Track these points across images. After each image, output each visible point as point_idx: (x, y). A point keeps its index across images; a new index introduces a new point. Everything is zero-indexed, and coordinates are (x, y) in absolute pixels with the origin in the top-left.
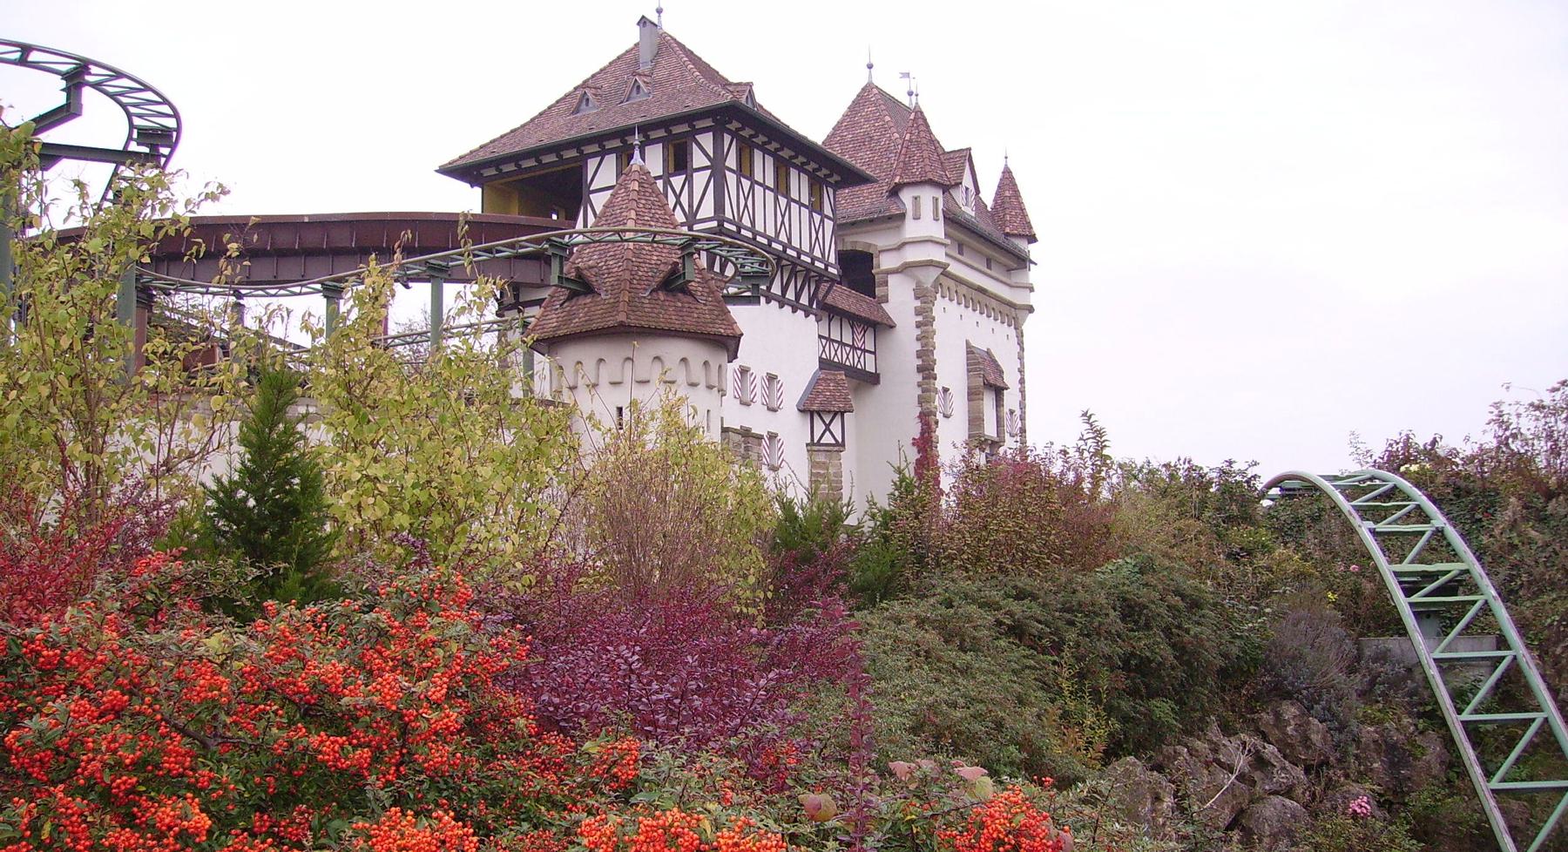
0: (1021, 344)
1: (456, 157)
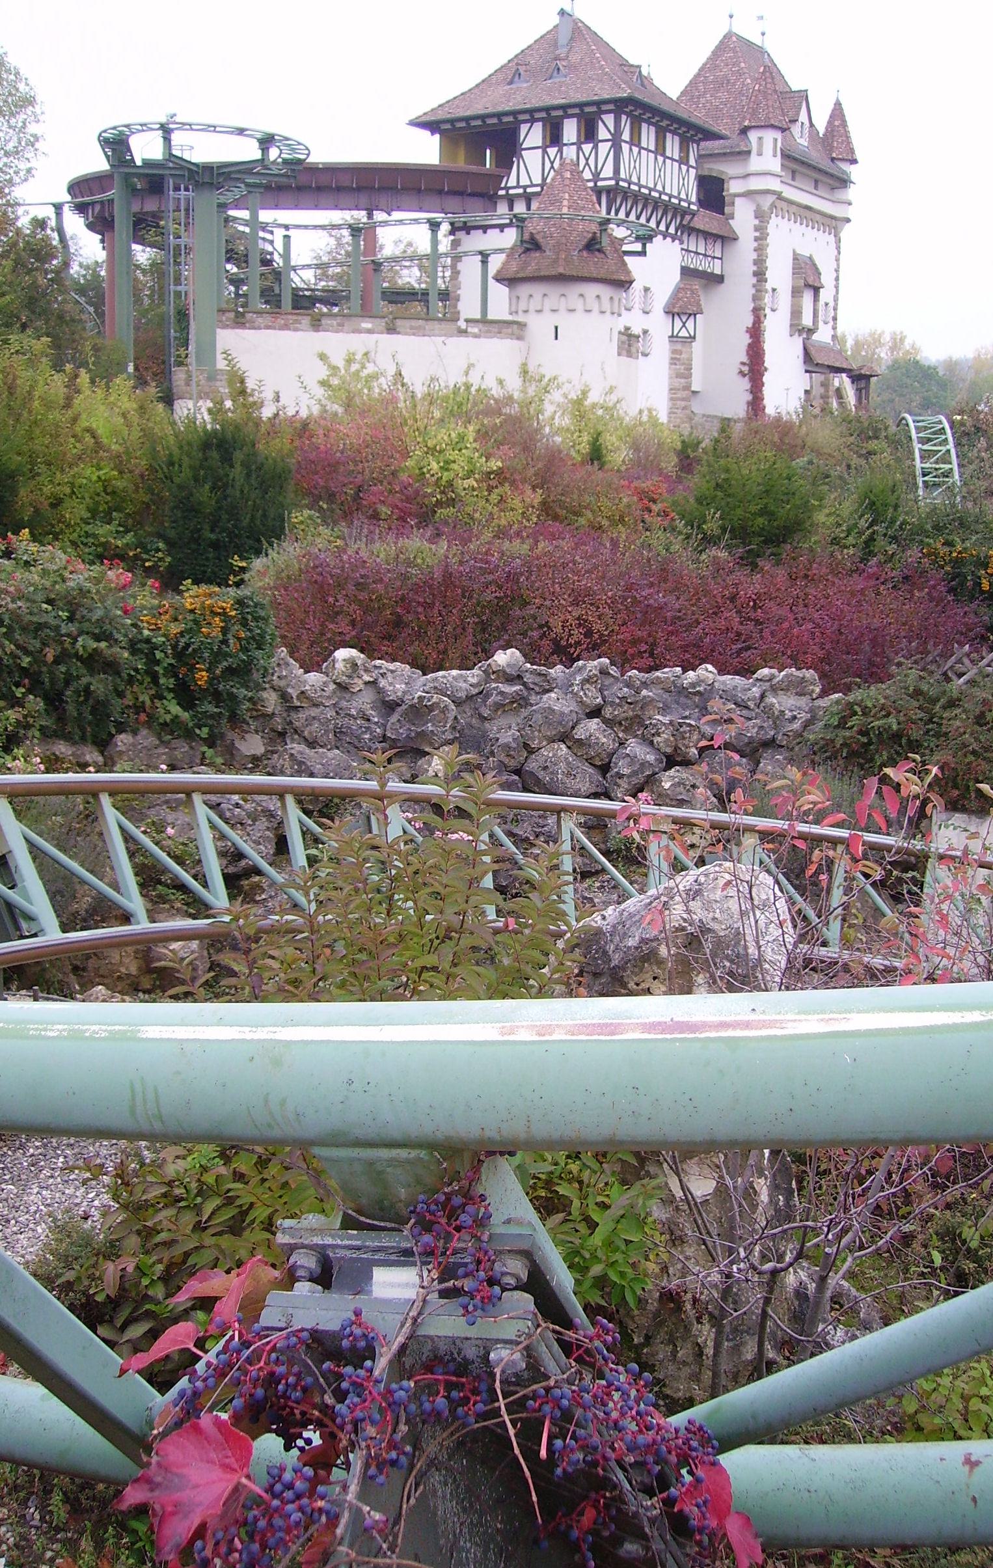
0: (838, 248)
1: (420, 113)
